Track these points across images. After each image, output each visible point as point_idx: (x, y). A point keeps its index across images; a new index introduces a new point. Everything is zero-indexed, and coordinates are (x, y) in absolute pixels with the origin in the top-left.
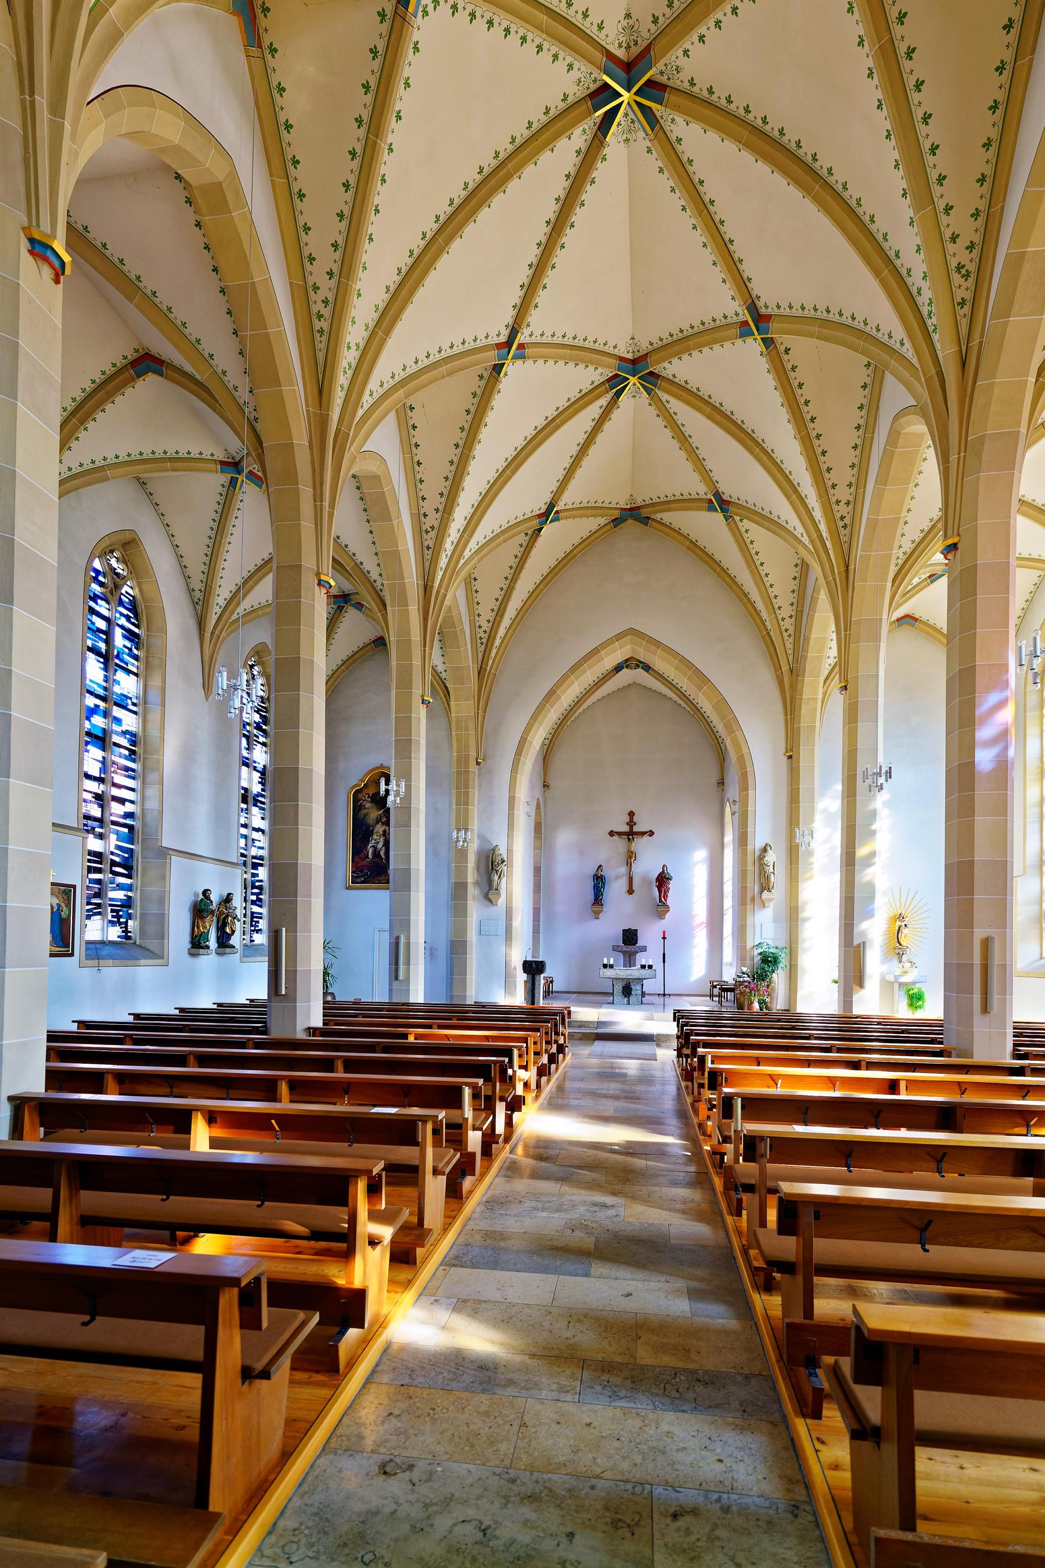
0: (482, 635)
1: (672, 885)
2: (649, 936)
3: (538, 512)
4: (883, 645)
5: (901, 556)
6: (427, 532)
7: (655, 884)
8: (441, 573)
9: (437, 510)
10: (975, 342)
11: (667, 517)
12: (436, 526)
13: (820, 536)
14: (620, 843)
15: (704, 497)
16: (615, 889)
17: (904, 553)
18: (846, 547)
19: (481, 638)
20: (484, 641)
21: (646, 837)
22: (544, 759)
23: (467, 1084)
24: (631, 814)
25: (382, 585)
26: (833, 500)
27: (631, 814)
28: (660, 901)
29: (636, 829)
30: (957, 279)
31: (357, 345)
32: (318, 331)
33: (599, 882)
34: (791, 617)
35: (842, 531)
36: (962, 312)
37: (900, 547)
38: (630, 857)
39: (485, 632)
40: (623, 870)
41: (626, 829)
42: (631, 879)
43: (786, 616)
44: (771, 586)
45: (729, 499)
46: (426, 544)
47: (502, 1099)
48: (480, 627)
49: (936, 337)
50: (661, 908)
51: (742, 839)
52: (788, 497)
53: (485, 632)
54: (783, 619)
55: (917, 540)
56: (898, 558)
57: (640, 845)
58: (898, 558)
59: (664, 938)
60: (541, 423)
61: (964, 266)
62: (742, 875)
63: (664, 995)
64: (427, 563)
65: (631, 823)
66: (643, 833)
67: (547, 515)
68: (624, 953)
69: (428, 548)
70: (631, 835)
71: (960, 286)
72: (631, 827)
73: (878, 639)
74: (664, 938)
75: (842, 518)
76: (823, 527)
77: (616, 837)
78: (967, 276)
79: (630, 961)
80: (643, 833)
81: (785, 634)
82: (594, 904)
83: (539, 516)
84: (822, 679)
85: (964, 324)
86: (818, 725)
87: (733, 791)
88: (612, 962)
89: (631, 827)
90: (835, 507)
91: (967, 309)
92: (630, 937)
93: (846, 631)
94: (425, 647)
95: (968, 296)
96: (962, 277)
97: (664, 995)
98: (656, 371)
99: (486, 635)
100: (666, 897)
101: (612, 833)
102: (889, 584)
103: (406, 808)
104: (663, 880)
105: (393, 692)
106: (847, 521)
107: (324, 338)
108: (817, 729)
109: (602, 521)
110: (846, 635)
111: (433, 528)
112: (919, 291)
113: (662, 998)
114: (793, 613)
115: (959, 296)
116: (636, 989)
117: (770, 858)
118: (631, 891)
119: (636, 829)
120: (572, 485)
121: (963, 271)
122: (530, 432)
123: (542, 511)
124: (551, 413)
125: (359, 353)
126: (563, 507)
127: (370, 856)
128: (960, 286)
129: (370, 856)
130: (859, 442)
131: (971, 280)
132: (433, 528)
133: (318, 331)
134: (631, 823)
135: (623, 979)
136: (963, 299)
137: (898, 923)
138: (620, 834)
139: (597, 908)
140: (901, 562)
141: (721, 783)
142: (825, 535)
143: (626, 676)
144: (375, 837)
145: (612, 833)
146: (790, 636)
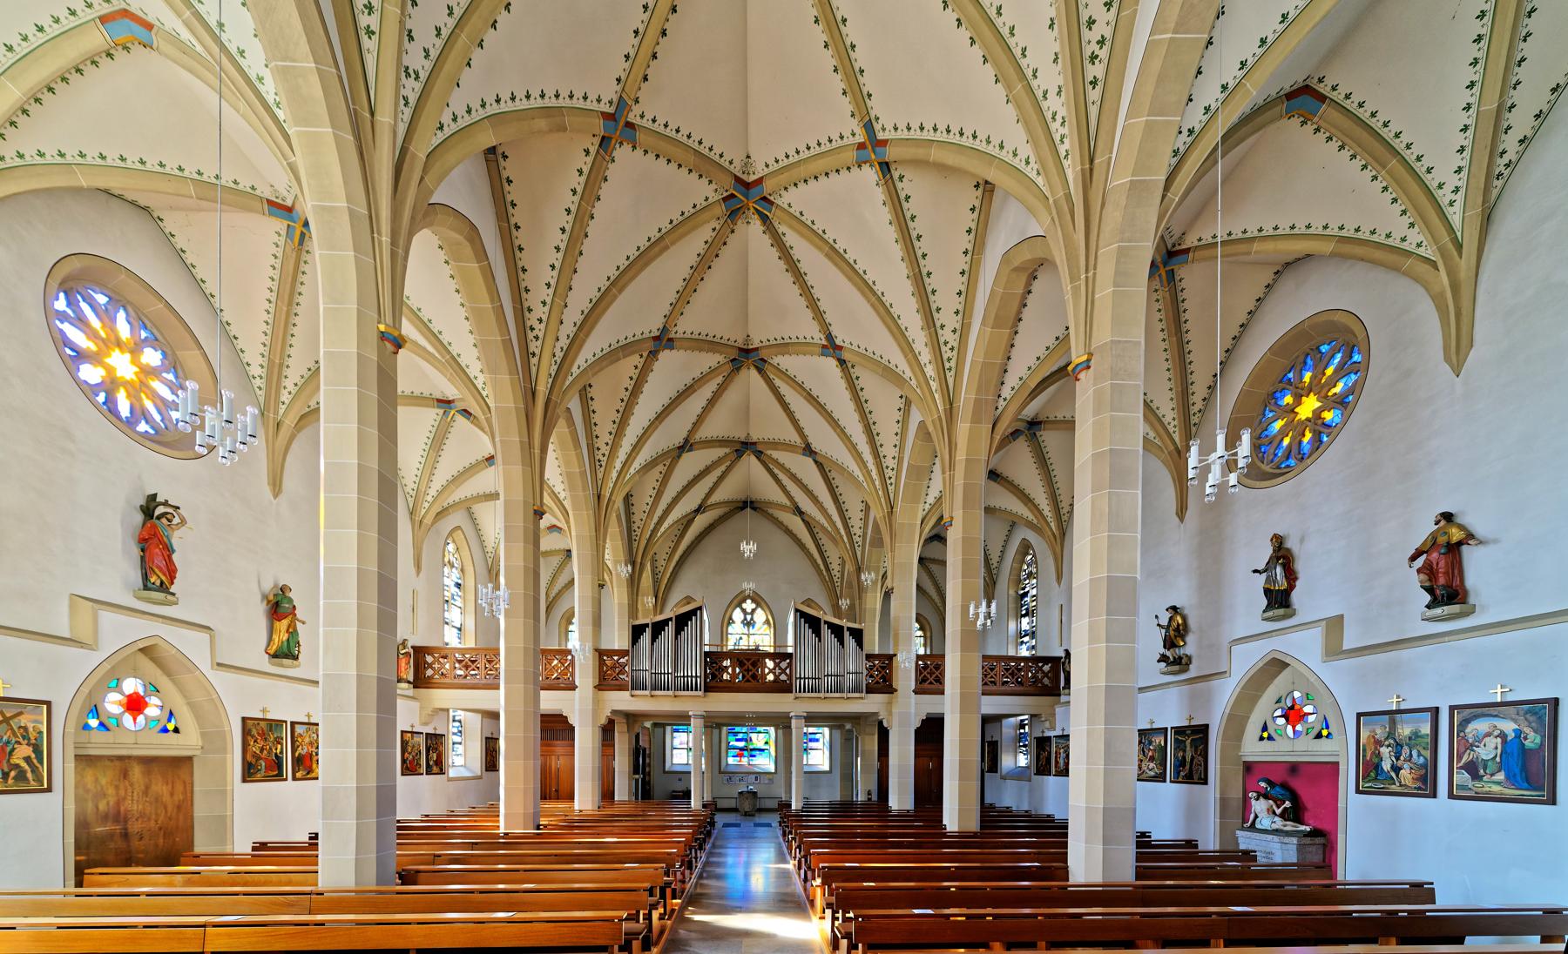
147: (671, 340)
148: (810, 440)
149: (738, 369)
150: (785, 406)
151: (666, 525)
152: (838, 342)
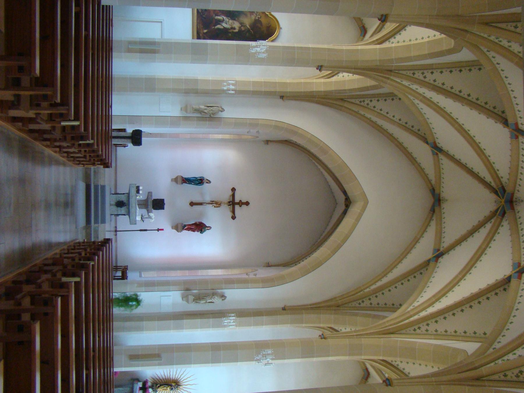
0: (366, 102)
1: (197, 234)
2: (157, 218)
3: (437, 142)
4: (346, 358)
5: (397, 363)
6: (423, 73)
7: (198, 221)
8: (399, 81)
9: (435, 81)
10: (486, 383)
11: (433, 223)
12: (426, 80)
13: (411, 316)
14: (226, 196)
15: (442, 246)
16: (193, 192)
17: (398, 365)
18: (404, 331)
19: (364, 101)
20: (362, 104)
21: (230, 214)
22: (286, 141)
23: (81, 123)
24: (247, 204)
25: (393, 43)
26: (429, 322)
27: (247, 204)
28: (185, 226)
29: (237, 207)
30: (516, 371)
31: (510, 46)
32: (516, 25)
33: (200, 181)
34: (371, 304)
35: (412, 328)
36: (501, 376)
37: (401, 362)
38: (217, 204)
39: (368, 104)
40: (208, 199)
41: (237, 200)
42: (201, 204)
43: (372, 301)
44: (390, 290)
45: (439, 261)
46: (416, 72)
47: (37, 114)
48: (371, 101)
49: (492, 364)
50: (181, 227)
51: (230, 282)
52: (434, 296)
53: (368, 104)
54: (370, 299)
55: (404, 371)
56: (396, 361)
57: (226, 210)
58: (396, 361)
59: (158, 230)
60: (482, 146)
61: (521, 374)
62: (204, 282)
63: (116, 231)
64: (404, 72)
65: (241, 204)
66: (233, 212)
67: (437, 149)
68: (146, 201)
69: (414, 74)
70: (233, 203)
71: (513, 373)
72: (238, 204)
73: (350, 355)
74: (158, 230)
75: (419, 328)
76: (416, 317)
77: (231, 193)
78: (517, 376)
79: (143, 204)
80: (233, 212)
81: (360, 301)
82: (182, 177)
83: (435, 143)
84: (332, 326)
85: (496, 377)
86: (304, 325)
87: (264, 273)
88: (141, 192)
89: (238, 204)
90: (425, 324)
91: (503, 378)
92: (159, 204)
93: (356, 335)
94: (355, 69)
95: (509, 378)
96: (517, 374)
97: (116, 231)
98: (506, 215)
99: (366, 105)
100: (188, 229)
101: (233, 190)
102: (381, 358)
103: (247, 59)
104: (200, 227)
105: (326, 46)
106: (418, 331)
107: (512, 29)
108: (301, 325)
109: (433, 182)
110: (353, 336)
111: (425, 77)
112: (515, 354)
113: (113, 229)
114: (373, 305)
115: (509, 373)
116: (123, 210)
117: (217, 300)
118: (192, 204)
119: (237, 207)
120: (452, 165)
121: (519, 374)
122: (477, 139)
123: (438, 145)
124: (487, 153)
125: (507, 47)
126: (440, 158)
127: (217, 17)
128: (513, 373)
129: (217, 17)
130: (458, 334)
131: (515, 379)
132: (425, 77)
133: (516, 25)
134: (241, 204)
135: (129, 201)
136: (507, 375)
137: (173, 384)
138: (233, 196)
139: (180, 180)
140: (393, 363)
141: (268, 265)
142: (365, 291)
143: (341, 198)
144: (231, 21)
145: (233, 190)
146: (360, 304)
147: (517, 137)
148: (445, 257)
149: (496, 192)
150: (471, 233)
151: (421, 105)
152: (440, 259)
